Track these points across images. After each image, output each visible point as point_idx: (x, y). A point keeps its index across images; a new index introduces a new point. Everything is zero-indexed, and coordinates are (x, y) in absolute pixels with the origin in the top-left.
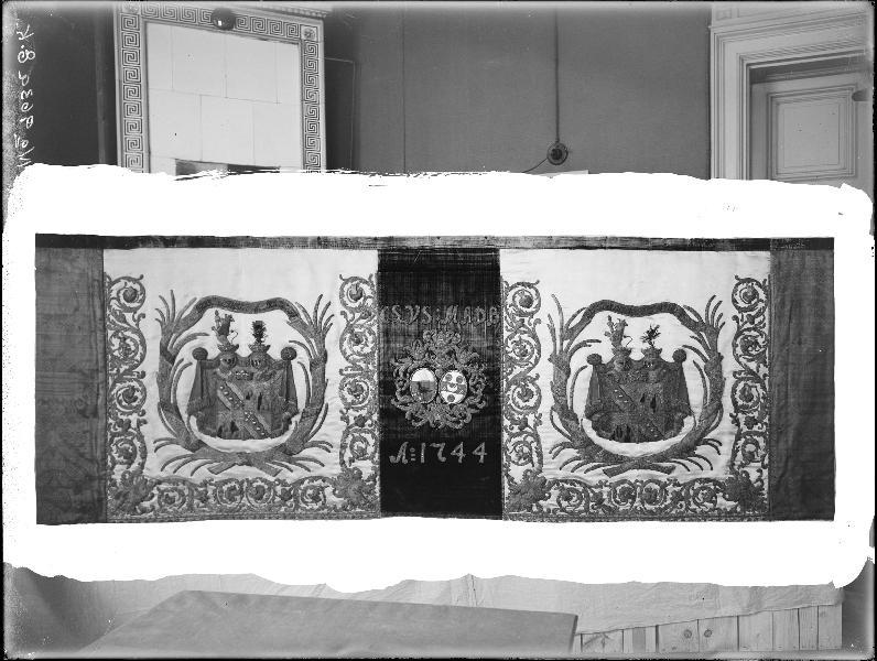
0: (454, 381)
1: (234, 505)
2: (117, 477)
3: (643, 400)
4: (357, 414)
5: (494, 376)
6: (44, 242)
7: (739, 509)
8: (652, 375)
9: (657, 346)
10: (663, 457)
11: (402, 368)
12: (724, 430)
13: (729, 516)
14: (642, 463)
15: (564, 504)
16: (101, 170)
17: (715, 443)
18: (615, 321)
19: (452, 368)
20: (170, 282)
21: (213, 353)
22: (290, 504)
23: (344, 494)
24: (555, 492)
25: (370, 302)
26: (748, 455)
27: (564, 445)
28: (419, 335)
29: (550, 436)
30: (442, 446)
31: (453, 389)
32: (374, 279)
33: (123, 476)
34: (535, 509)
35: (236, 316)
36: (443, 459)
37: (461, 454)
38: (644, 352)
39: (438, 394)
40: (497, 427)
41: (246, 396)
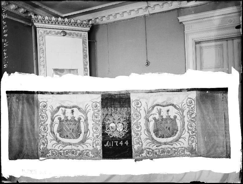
0: (120, 126)
1: (67, 155)
2: (41, 148)
3: (166, 128)
4: (97, 135)
5: (129, 124)
6: (8, 92)
7: (190, 154)
8: (169, 122)
9: (169, 115)
10: (171, 142)
11: (107, 123)
12: (186, 135)
13: (188, 156)
14: (165, 144)
15: (147, 154)
16: (33, 76)
17: (185, 138)
18: (158, 109)
19: (119, 123)
20: (52, 102)
21: (63, 118)
22: (81, 156)
23: (93, 154)
24: (145, 152)
25: (99, 108)
26: (192, 141)
27: (147, 139)
28: (111, 115)
29: (143, 136)
30: (117, 142)
31: (120, 128)
32: (195, 100)
33: (43, 148)
34: (140, 156)
35: (66, 109)
36: (118, 145)
37: (122, 144)
38: (166, 116)
39: (116, 129)
40: (130, 136)
41: (70, 128)
